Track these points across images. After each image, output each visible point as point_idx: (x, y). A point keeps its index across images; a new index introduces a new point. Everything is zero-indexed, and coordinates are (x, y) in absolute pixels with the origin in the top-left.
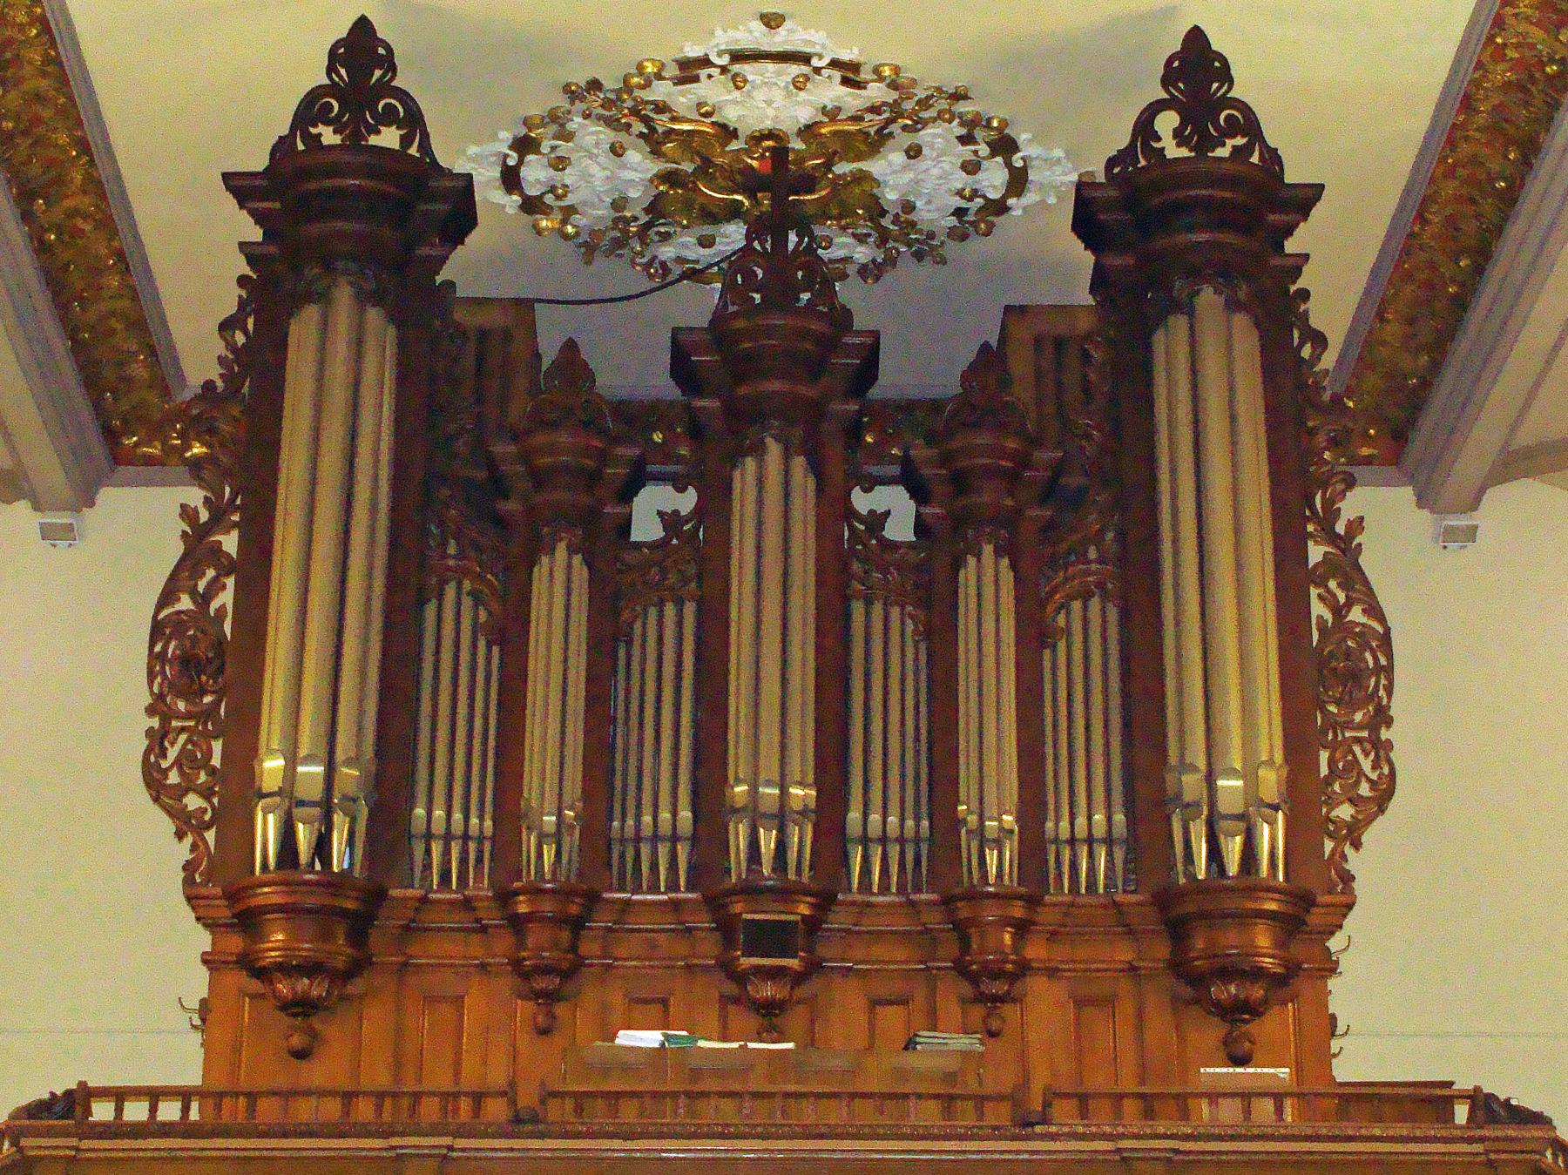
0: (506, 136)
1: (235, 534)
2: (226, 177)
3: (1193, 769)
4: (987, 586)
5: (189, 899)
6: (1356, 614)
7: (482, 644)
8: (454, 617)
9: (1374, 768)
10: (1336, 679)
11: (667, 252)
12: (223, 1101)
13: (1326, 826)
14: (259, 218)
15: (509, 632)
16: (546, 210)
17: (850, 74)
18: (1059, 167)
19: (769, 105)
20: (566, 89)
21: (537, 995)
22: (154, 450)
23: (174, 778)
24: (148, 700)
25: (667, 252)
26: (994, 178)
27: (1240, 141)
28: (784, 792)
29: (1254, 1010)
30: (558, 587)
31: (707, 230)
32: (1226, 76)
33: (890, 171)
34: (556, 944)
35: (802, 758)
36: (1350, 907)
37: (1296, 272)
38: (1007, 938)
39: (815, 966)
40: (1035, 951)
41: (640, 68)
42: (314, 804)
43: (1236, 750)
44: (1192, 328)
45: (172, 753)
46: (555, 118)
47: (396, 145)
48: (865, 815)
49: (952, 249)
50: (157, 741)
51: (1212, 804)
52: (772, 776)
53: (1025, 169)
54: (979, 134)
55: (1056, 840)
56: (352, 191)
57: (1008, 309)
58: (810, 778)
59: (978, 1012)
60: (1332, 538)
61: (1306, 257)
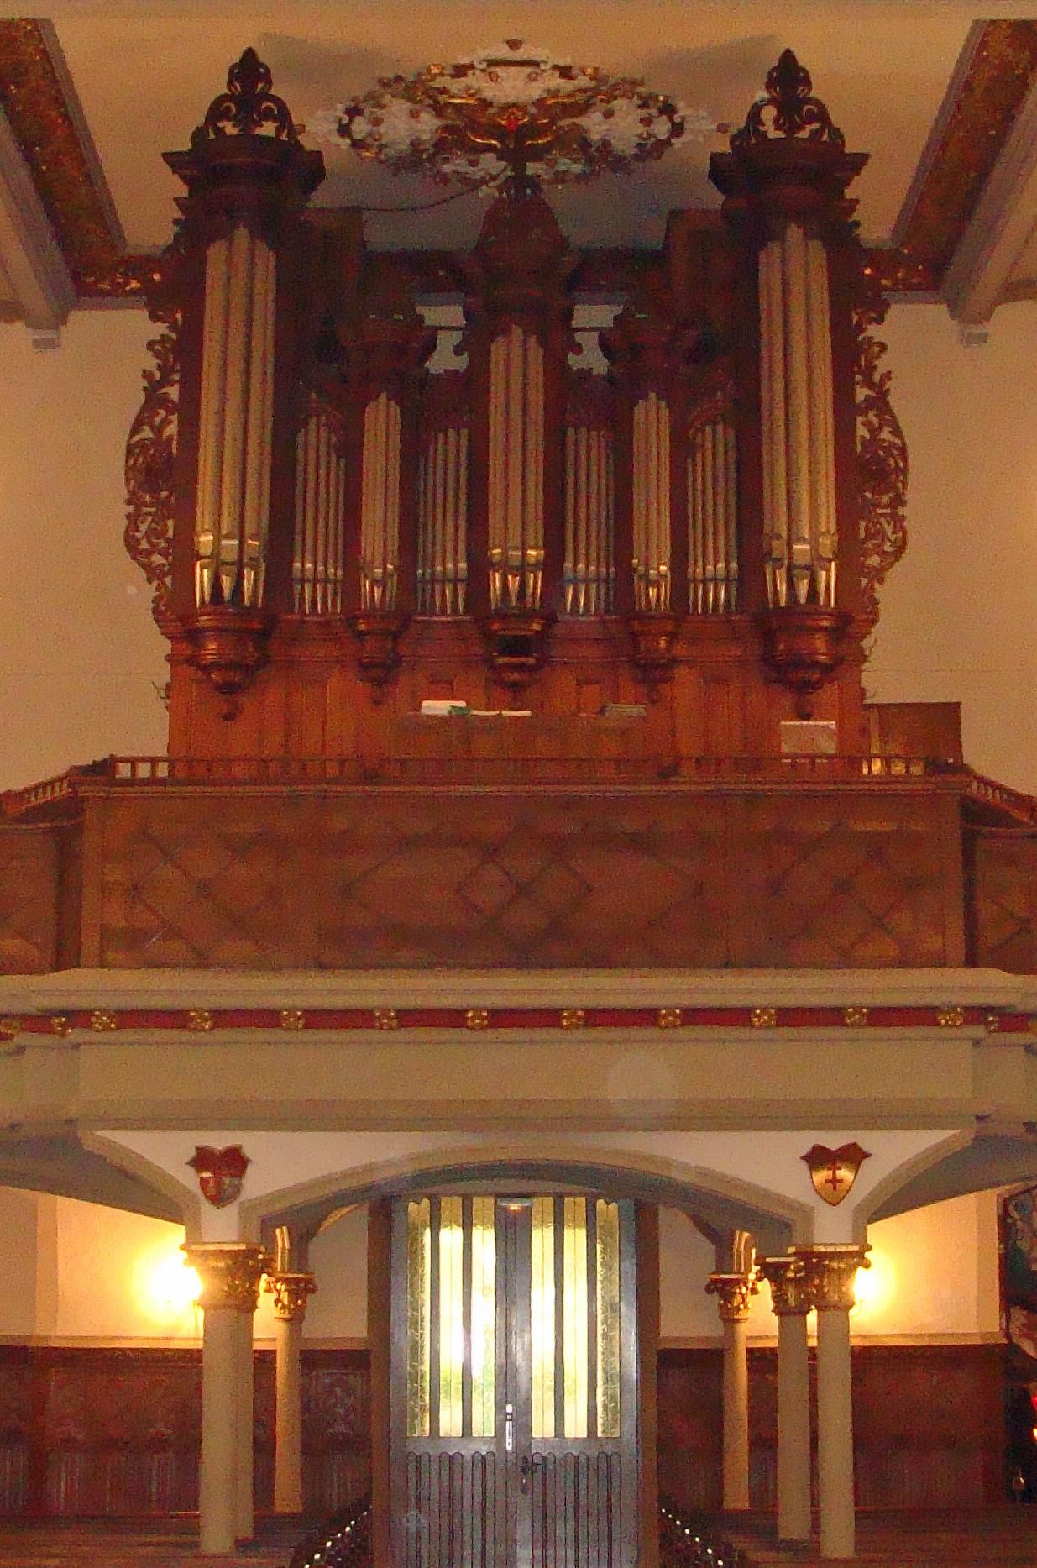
0: (340, 107)
1: (177, 386)
2: (163, 155)
3: (779, 537)
4: (652, 420)
5: (157, 621)
6: (885, 435)
7: (334, 458)
8: (315, 439)
9: (894, 532)
10: (871, 475)
11: (447, 168)
12: (190, 765)
13: (862, 569)
14: (187, 180)
15: (350, 450)
16: (367, 148)
17: (565, 72)
18: (705, 135)
19: (512, 88)
20: (380, 81)
21: (370, 680)
22: (105, 286)
23: (144, 545)
24: (127, 496)
25: (447, 168)
26: (662, 128)
27: (815, 126)
28: (524, 555)
29: (817, 686)
30: (382, 420)
31: (474, 157)
32: (807, 82)
33: (594, 125)
34: (384, 649)
35: (536, 531)
36: (874, 621)
37: (853, 210)
38: (662, 643)
39: (542, 662)
40: (680, 650)
41: (429, 70)
42: (232, 564)
43: (807, 520)
44: (784, 251)
45: (143, 528)
46: (372, 97)
47: (272, 134)
48: (575, 566)
49: (634, 165)
50: (134, 520)
51: (790, 558)
52: (517, 543)
53: (681, 124)
54: (651, 103)
55: (695, 580)
56: (245, 160)
57: (672, 213)
58: (541, 543)
59: (643, 689)
60: (869, 383)
61: (857, 201)
